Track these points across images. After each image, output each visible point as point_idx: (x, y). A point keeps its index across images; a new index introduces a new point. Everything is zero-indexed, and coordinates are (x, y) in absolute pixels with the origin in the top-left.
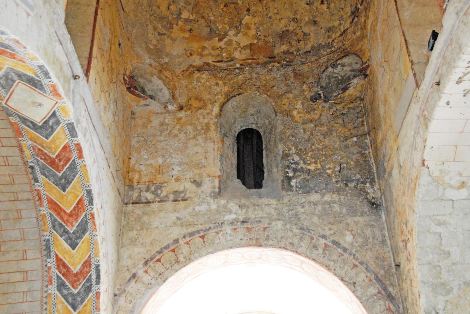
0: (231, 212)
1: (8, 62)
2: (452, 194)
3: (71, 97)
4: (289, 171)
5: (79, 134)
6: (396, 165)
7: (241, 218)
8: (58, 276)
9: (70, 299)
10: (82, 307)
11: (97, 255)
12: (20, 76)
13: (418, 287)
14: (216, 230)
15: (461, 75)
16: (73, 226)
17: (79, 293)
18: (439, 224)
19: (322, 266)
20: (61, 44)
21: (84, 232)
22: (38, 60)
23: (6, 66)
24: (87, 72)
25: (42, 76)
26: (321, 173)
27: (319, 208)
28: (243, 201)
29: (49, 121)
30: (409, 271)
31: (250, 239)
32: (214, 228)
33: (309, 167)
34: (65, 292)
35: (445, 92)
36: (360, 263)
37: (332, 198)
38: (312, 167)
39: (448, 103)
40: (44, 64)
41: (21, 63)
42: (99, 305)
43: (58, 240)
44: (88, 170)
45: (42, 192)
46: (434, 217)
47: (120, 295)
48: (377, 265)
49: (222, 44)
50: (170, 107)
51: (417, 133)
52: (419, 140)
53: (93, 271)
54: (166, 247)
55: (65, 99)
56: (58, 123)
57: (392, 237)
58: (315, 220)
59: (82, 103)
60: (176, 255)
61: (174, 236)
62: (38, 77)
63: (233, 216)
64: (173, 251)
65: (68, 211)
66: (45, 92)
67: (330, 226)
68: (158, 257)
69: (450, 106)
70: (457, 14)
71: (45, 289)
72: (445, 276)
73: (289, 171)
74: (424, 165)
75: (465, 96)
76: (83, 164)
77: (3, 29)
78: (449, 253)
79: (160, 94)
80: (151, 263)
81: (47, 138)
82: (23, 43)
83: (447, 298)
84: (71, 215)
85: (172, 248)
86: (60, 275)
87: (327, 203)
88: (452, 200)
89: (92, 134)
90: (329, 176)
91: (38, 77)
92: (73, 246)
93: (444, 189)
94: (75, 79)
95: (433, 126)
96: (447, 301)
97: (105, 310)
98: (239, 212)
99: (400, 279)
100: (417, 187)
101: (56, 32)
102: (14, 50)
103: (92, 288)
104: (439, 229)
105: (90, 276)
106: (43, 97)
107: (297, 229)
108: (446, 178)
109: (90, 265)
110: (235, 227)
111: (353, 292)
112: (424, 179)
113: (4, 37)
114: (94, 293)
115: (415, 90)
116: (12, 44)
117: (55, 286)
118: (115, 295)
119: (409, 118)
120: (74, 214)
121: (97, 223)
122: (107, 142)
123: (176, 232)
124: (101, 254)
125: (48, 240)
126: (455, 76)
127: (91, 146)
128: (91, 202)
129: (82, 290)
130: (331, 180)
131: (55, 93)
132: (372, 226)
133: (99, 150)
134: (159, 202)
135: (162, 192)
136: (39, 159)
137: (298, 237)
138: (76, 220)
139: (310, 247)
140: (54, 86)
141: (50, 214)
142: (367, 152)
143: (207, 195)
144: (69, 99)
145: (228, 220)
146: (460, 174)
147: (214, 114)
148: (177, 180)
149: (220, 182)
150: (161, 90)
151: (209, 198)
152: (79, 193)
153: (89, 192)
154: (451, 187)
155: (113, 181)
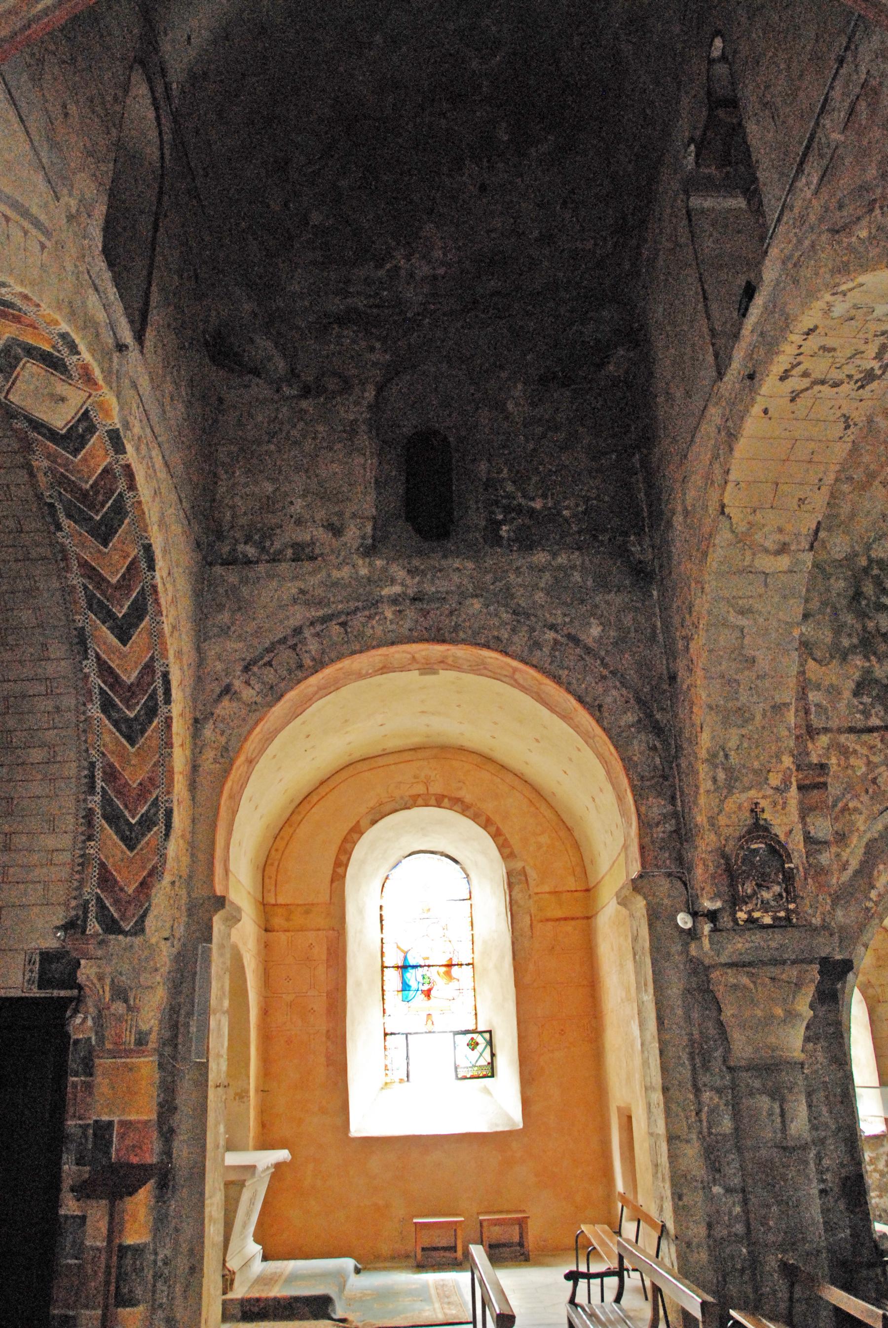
0: (393, 581)
1: (8, 329)
2: (766, 563)
3: (114, 385)
5: (129, 447)
6: (679, 508)
7: (411, 592)
9: (123, 727)
10: (143, 740)
11: (164, 654)
12: (30, 351)
13: (700, 714)
14: (367, 613)
16: (122, 607)
17: (136, 718)
19: (547, 677)
20: (97, 290)
21: (141, 618)
22: (60, 324)
23: (7, 335)
24: (140, 337)
25: (65, 351)
26: (552, 516)
27: (547, 575)
28: (416, 562)
29: (77, 427)
30: (689, 688)
32: (364, 608)
33: (532, 504)
34: (115, 715)
35: (761, 393)
36: (611, 672)
38: (538, 505)
39: (766, 411)
41: (30, 330)
43: (97, 628)
44: (146, 510)
46: (735, 601)
47: (206, 719)
49: (381, 273)
50: (287, 390)
51: (716, 457)
52: (717, 470)
53: (159, 682)
54: (283, 641)
55: (105, 390)
56: (91, 429)
58: (540, 597)
59: (132, 392)
61: (293, 622)
62: (59, 351)
63: (397, 589)
64: (294, 647)
65: (114, 580)
66: (70, 377)
67: (565, 609)
68: (266, 659)
69: (768, 416)
70: (784, 263)
71: (82, 708)
72: (744, 698)
75: (793, 400)
76: (135, 500)
77: (14, 290)
78: (753, 660)
79: (270, 366)
80: (255, 669)
81: (75, 456)
82: (35, 298)
83: (744, 731)
84: (118, 587)
85: (290, 642)
86: (106, 688)
87: (560, 568)
88: (764, 573)
90: (566, 520)
91: (59, 351)
92: (124, 638)
93: (754, 554)
94: (120, 351)
95: (742, 447)
96: (743, 736)
97: (182, 745)
98: (409, 582)
99: (674, 697)
100: (711, 550)
101: (88, 272)
102: (20, 310)
103: (157, 710)
104: (743, 621)
105: (155, 690)
106: (67, 387)
107: (507, 612)
108: (758, 537)
109: (154, 672)
110: (401, 608)
111: (597, 721)
112: (724, 536)
113: (3, 290)
115: (715, 382)
116: (18, 302)
117: (97, 705)
118: (196, 721)
119: (704, 427)
120: (125, 584)
121: (162, 601)
122: (176, 459)
123: (298, 615)
124: (171, 654)
125: (83, 628)
127: (149, 468)
128: (151, 567)
131: (88, 378)
132: (636, 609)
133: (162, 474)
134: (268, 562)
135: (272, 544)
136: (62, 491)
137: (508, 627)
139: (529, 643)
140: (86, 368)
141: (83, 585)
142: (633, 480)
143: (353, 551)
144: (111, 388)
145: (389, 596)
146: (780, 530)
148: (299, 522)
149: (374, 529)
150: (270, 359)
151: (355, 557)
153: (148, 549)
154: (766, 551)
155: (186, 528)
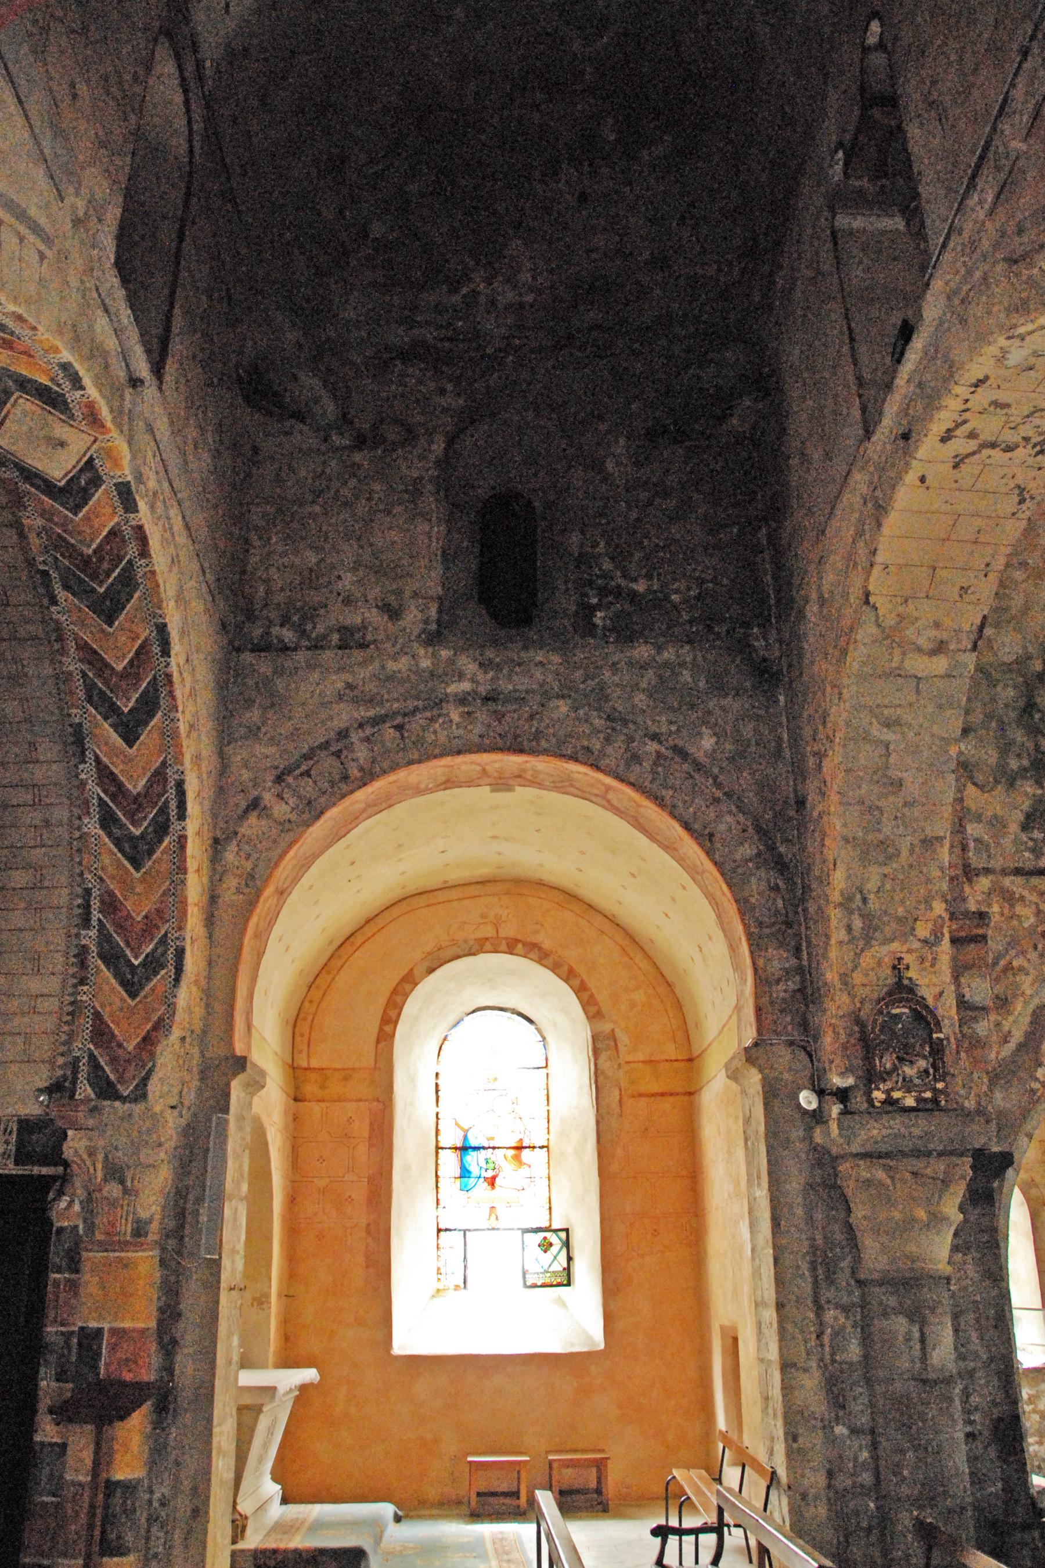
0: (461, 676)
2: (919, 665)
3: (126, 428)
4: (591, 593)
5: (142, 505)
6: (814, 596)
7: (482, 690)
8: (100, 799)
9: (127, 847)
10: (150, 863)
11: (179, 759)
13: (833, 848)
14: (428, 714)
15: (952, 425)
16: (128, 700)
17: (143, 836)
18: (888, 724)
22: (60, 352)
24: (158, 370)
25: (67, 385)
26: (658, 601)
28: (490, 654)
29: (78, 478)
31: (500, 735)
32: (425, 708)
34: (117, 832)
35: (918, 456)
36: (725, 794)
37: (678, 656)
38: (641, 587)
39: (923, 479)
40: (71, 359)
41: (24, 358)
42: (185, 861)
43: (97, 725)
44: (161, 581)
45: (64, 625)
48: (763, 800)
49: (456, 299)
50: (337, 440)
51: (860, 533)
52: (862, 550)
53: (172, 793)
55: (114, 433)
56: (96, 481)
57: (795, 740)
58: (640, 700)
59: (148, 437)
60: (342, 764)
61: (338, 724)
62: (59, 385)
63: (466, 686)
64: (338, 754)
65: (119, 667)
66: (72, 417)
67: (671, 716)
68: (304, 768)
69: (926, 485)
70: (949, 298)
73: (591, 593)
74: (867, 602)
75: (956, 466)
76: (148, 569)
78: (900, 783)
79: (317, 410)
81: (76, 514)
82: (31, 320)
83: (886, 870)
84: (124, 675)
85: (334, 748)
87: (666, 664)
88: (916, 677)
89: (168, 504)
91: (59, 385)
92: (130, 737)
93: (904, 654)
94: (134, 386)
95: (892, 522)
96: (885, 876)
97: (198, 871)
98: (480, 677)
99: (801, 827)
100: (851, 647)
101: (97, 290)
102: (12, 333)
103: (169, 827)
104: (888, 735)
105: (166, 802)
106: (67, 429)
107: (600, 717)
111: (708, 853)
112: (867, 631)
114: (174, 838)
117: (96, 819)
119: (846, 497)
121: (178, 693)
122: (199, 520)
123: (344, 715)
125: (80, 725)
126: (938, 426)
127: (165, 531)
128: (166, 652)
129: (150, 830)
130: (680, 616)
131: (93, 419)
132: (758, 718)
134: (309, 649)
135: (314, 628)
137: (601, 736)
138: (136, 688)
140: (91, 406)
142: (758, 559)
143: (413, 638)
145: (456, 695)
146: (937, 625)
147: (432, 457)
148: (348, 601)
151: (415, 645)
152: (140, 630)
153: (162, 629)
154: (919, 650)
155: (209, 605)
